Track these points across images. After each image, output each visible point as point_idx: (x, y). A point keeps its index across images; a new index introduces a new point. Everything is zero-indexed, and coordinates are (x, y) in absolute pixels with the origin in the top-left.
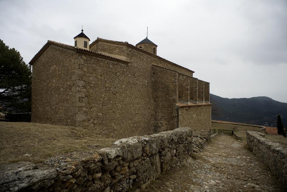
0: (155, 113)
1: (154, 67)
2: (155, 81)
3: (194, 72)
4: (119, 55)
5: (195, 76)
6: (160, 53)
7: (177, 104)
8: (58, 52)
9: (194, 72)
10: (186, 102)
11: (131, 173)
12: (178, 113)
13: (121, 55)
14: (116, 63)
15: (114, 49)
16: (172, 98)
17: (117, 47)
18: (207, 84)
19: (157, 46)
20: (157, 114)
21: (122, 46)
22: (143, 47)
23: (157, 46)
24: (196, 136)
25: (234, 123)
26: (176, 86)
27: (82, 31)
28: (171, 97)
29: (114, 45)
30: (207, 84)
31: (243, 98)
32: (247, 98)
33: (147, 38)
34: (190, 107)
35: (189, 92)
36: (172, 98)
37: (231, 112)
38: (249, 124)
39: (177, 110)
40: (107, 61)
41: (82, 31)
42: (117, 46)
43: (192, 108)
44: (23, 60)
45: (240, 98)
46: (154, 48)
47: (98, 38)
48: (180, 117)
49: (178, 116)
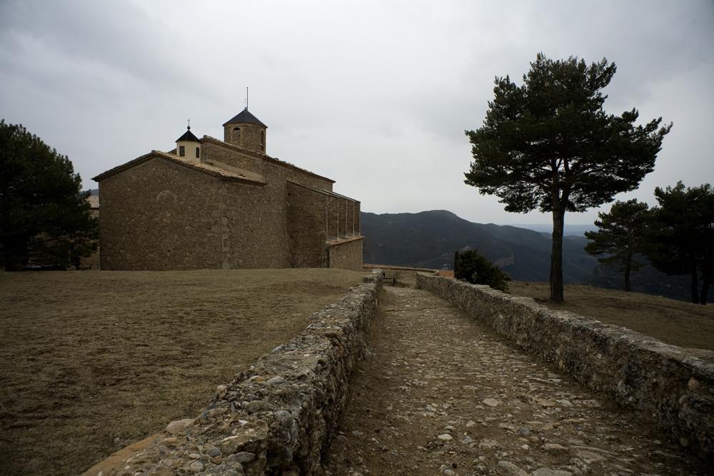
0: (293, 254)
1: (291, 184)
2: (291, 206)
3: (335, 182)
4: (249, 170)
5: (336, 189)
6: (275, 148)
7: (327, 242)
8: (176, 172)
9: (335, 182)
10: (334, 238)
11: (45, 384)
12: (328, 256)
13: (252, 171)
14: (252, 186)
15: (239, 160)
16: (319, 233)
17: (244, 157)
18: (358, 203)
19: (267, 127)
20: (296, 257)
21: (254, 158)
22: (241, 128)
23: (267, 127)
24: (333, 288)
25: (393, 267)
26: (325, 215)
27: (189, 128)
28: (317, 231)
29: (239, 153)
30: (358, 203)
31: (404, 212)
32: (412, 213)
33: (246, 109)
34: (340, 245)
35: (338, 222)
36: (319, 233)
37: (380, 245)
38: (416, 267)
39: (328, 251)
40: (246, 185)
41: (189, 128)
42: (244, 155)
43: (342, 246)
44: (58, 152)
45: (397, 213)
46: (262, 132)
47: (205, 136)
48: (331, 260)
49: (328, 259)
